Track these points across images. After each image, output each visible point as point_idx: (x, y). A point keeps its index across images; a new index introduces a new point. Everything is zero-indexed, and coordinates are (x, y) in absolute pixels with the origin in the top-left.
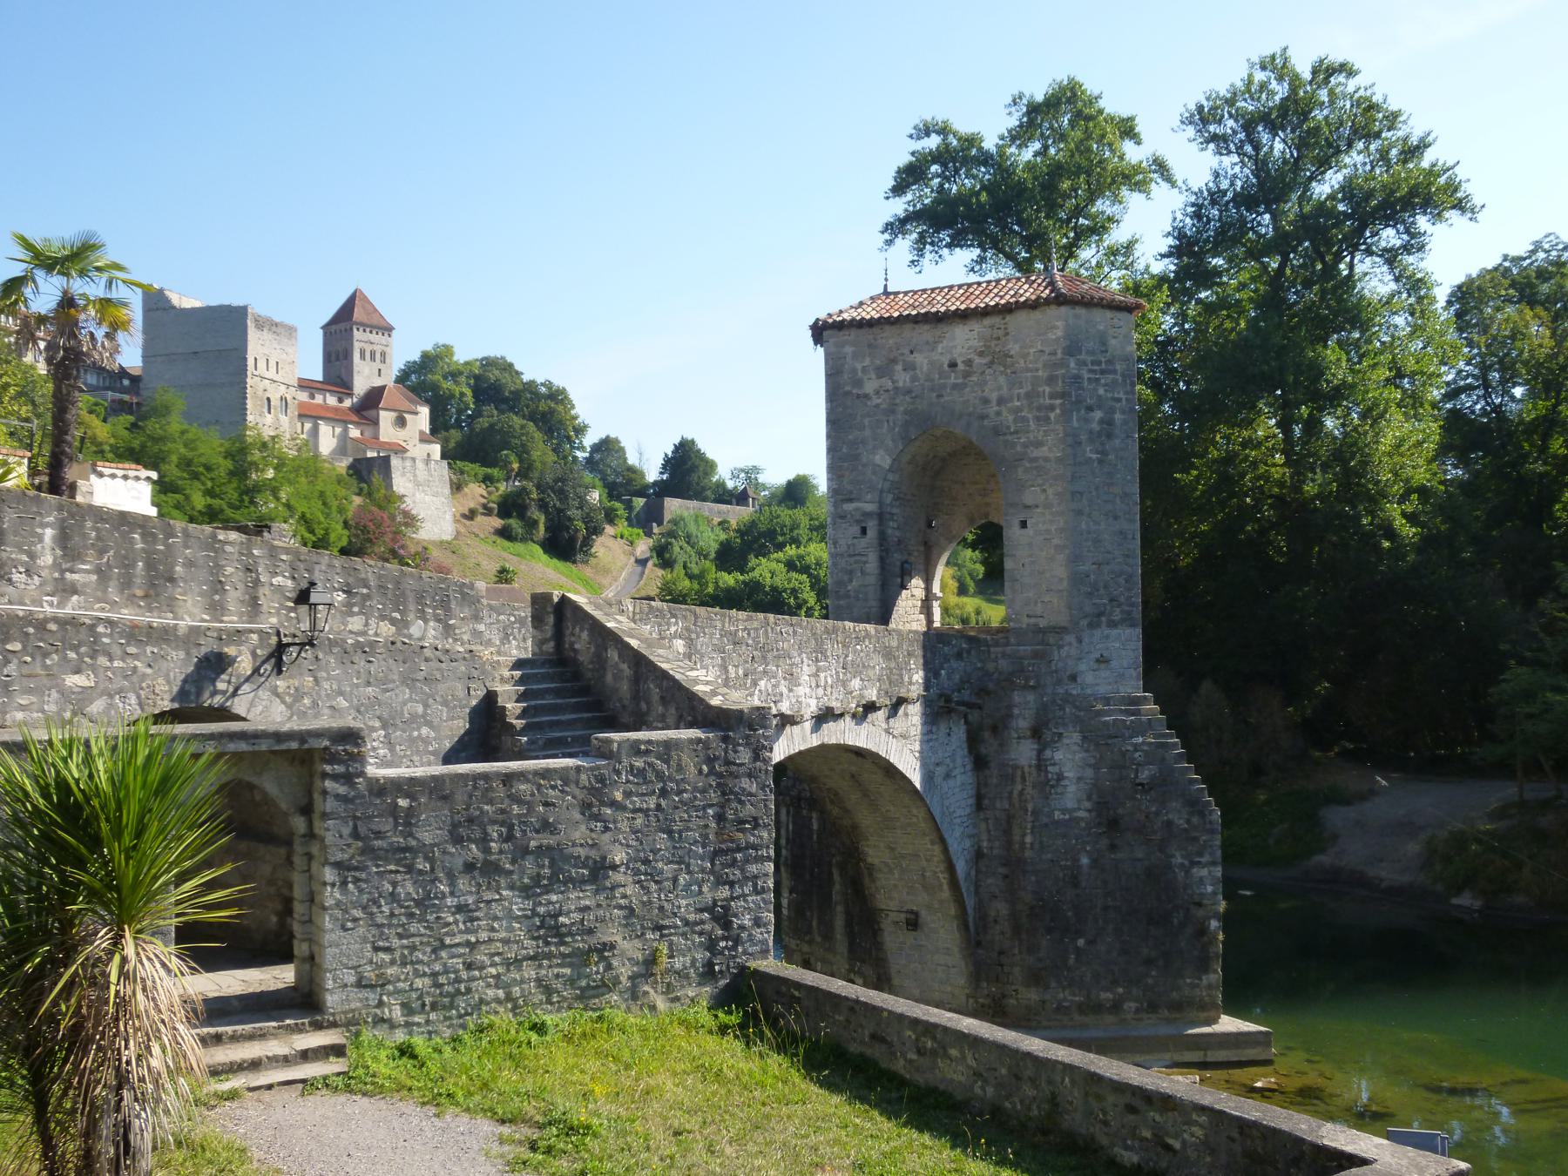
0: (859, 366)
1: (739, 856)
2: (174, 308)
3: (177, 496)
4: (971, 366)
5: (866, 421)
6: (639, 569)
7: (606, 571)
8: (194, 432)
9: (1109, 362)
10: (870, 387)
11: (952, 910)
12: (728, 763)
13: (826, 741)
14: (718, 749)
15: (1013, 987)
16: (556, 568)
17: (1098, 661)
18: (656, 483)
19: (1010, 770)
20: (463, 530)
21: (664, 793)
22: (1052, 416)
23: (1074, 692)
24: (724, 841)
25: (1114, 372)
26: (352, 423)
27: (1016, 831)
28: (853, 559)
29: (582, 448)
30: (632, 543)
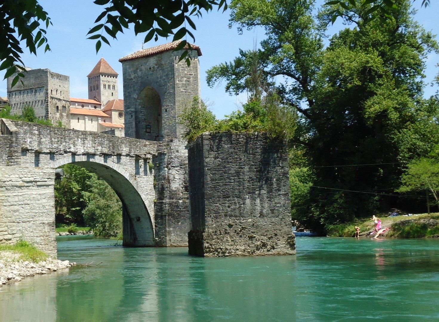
0: (130, 71)
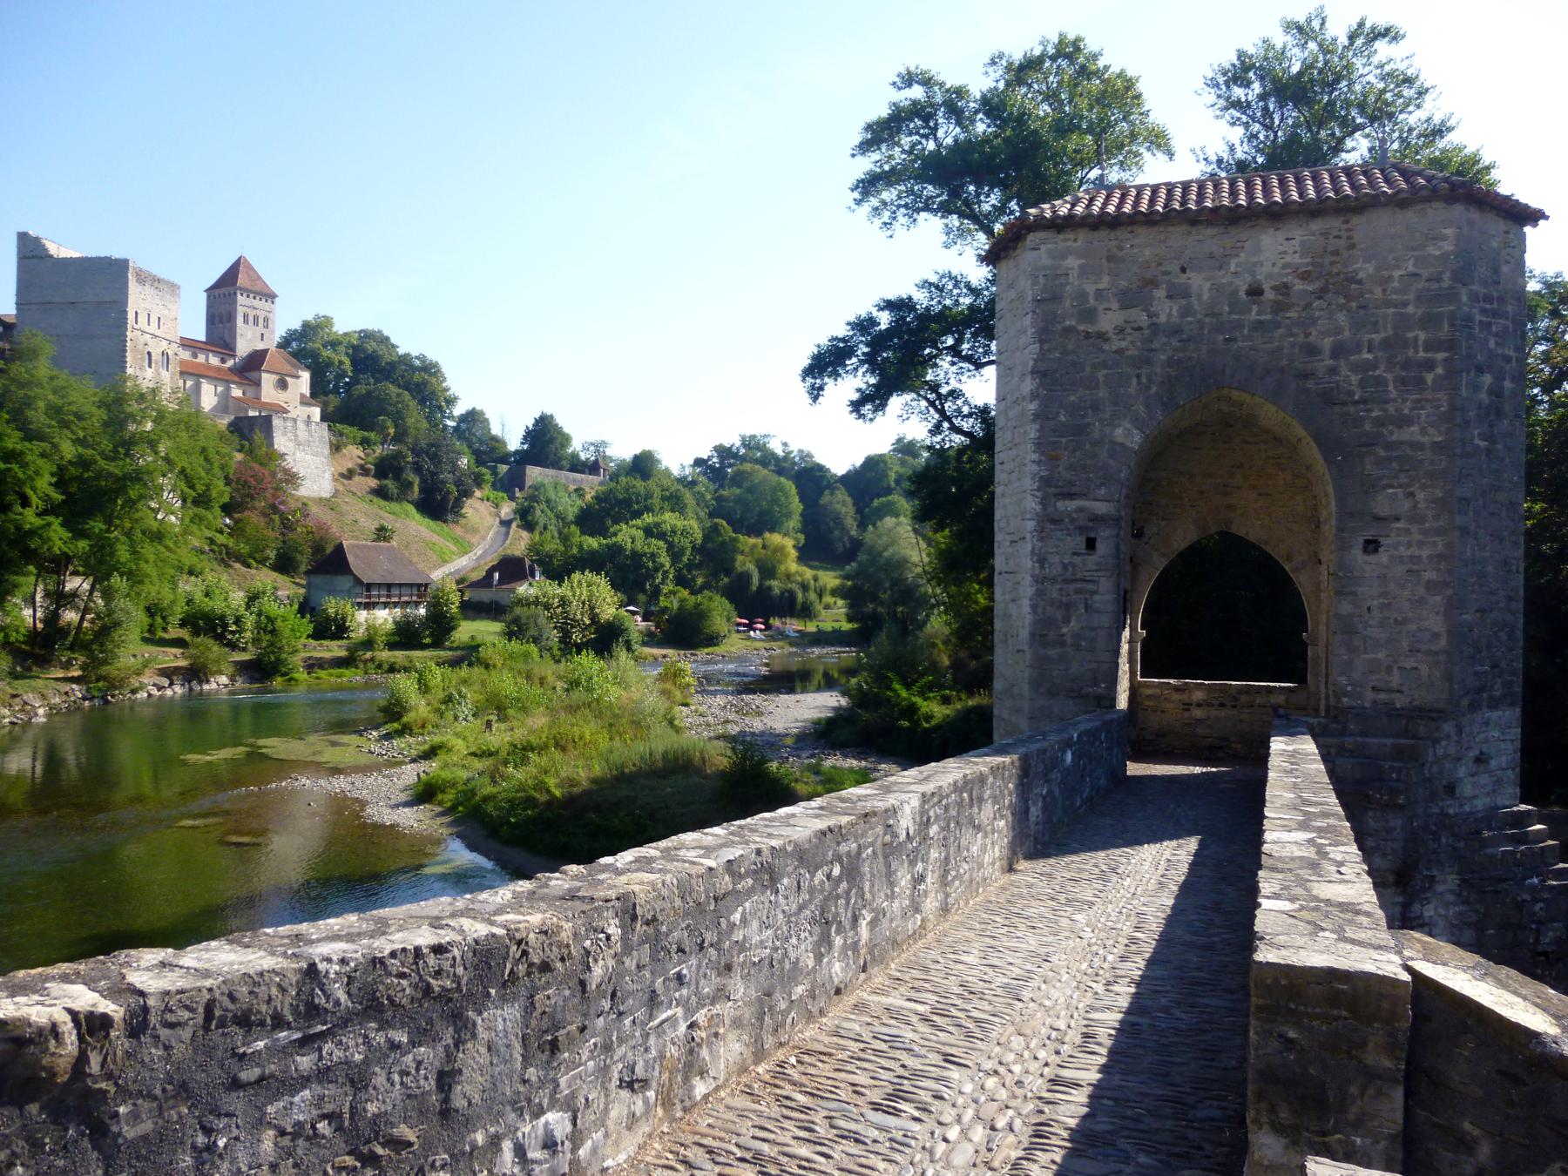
0: (1090, 289)
2: (51, 256)
3: (43, 444)
4: (1286, 295)
5: (1101, 375)
6: (503, 529)
7: (474, 531)
8: (64, 378)
9: (1501, 299)
10: (1108, 321)
16: (428, 527)
18: (517, 452)
20: (341, 488)
22: (1429, 378)
23: (1451, 811)
26: (234, 383)
28: (1072, 587)
29: (451, 417)
30: (497, 506)
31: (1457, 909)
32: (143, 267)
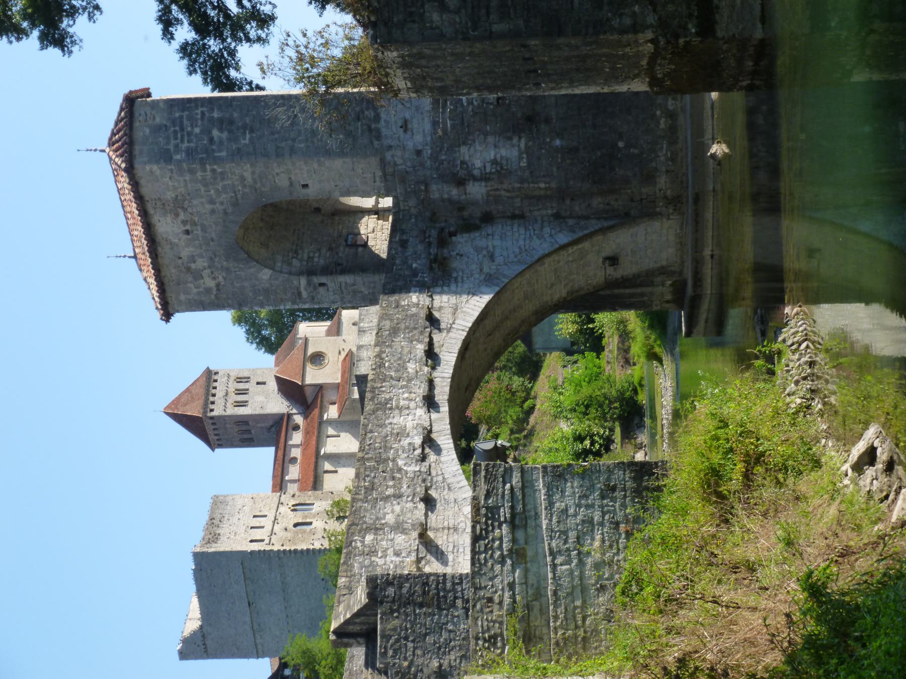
0: (195, 291)
1: (442, 594)
2: (201, 627)
4: (187, 221)
9: (174, 123)
10: (211, 283)
11: (599, 238)
12: (393, 601)
13: (446, 397)
14: (386, 606)
15: (658, 191)
17: (405, 131)
19: (491, 198)
21: (406, 638)
23: (429, 152)
24: (433, 604)
25: (181, 117)
26: (321, 416)
27: (537, 193)
28: (344, 291)
31: (478, 146)
32: (200, 538)
